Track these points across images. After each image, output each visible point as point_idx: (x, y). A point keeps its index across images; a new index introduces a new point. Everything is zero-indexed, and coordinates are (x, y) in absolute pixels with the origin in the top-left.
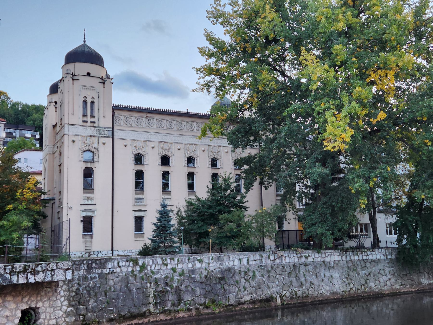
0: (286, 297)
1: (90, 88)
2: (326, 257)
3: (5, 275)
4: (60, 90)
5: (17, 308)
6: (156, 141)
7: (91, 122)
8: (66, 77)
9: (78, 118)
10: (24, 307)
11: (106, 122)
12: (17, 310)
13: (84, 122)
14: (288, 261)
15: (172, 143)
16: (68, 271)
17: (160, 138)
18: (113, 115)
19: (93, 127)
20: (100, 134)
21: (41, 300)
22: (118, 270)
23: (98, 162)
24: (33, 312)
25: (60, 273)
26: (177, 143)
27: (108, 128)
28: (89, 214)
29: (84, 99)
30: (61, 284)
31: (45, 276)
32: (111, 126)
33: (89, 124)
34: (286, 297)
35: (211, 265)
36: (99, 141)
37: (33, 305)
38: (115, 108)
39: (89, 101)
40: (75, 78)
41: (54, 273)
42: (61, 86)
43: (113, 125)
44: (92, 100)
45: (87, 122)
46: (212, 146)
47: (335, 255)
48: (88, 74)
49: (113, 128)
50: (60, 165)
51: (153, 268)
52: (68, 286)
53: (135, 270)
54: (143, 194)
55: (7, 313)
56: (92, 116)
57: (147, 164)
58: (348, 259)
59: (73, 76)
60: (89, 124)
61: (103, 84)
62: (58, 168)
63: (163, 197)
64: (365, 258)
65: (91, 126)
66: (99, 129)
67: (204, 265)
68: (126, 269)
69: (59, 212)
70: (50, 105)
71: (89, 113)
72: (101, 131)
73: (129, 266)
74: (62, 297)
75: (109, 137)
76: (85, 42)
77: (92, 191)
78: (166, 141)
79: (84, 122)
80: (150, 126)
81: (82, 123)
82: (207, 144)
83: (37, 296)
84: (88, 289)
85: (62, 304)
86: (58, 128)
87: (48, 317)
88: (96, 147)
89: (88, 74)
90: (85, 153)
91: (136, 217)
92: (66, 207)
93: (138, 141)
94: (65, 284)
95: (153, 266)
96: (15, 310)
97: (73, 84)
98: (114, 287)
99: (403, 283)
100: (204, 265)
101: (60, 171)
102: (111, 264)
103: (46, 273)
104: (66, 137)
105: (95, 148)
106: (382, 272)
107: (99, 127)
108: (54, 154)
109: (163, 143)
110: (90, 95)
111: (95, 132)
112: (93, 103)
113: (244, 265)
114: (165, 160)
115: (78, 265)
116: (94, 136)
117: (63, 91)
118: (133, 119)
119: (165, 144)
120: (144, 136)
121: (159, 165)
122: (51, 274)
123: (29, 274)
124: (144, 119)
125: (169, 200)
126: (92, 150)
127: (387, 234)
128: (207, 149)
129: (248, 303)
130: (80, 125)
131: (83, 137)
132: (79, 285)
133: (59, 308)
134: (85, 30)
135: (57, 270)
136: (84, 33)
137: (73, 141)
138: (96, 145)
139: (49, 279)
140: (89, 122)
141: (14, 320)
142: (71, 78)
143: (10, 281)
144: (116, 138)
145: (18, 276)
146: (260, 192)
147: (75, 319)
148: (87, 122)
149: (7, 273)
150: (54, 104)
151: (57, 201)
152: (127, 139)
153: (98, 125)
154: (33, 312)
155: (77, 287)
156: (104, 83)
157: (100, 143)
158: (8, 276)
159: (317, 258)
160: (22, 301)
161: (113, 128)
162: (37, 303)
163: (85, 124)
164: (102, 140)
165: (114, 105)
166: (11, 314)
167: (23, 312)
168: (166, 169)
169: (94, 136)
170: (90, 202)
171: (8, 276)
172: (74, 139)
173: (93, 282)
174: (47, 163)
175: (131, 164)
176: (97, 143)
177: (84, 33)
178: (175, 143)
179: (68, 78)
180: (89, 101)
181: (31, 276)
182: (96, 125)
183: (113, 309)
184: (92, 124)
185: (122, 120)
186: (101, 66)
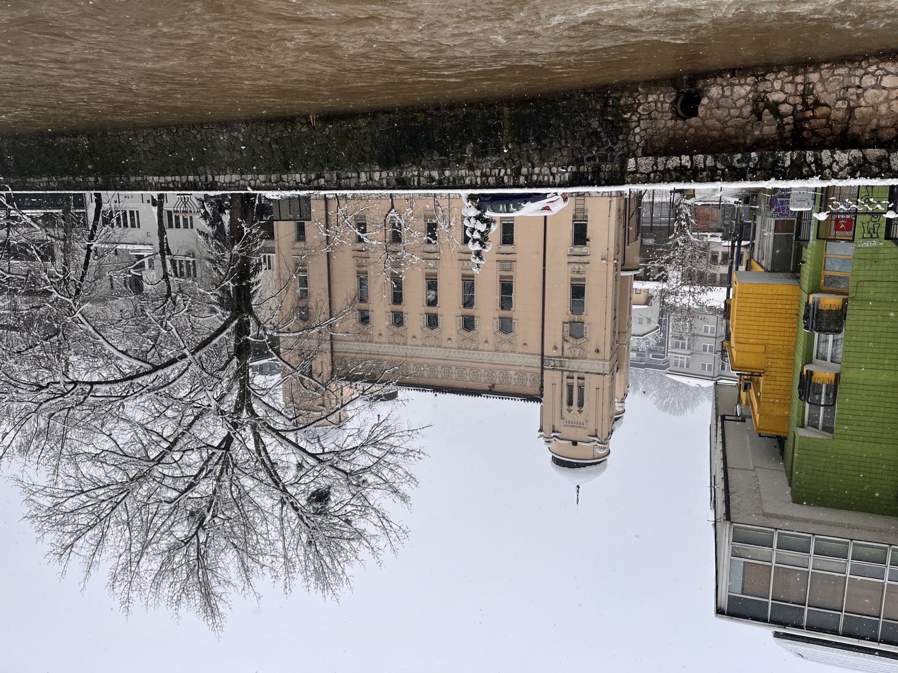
0: (301, 123)
2: (239, 181)
3: (723, 167)
5: (703, 119)
7: (572, 378)
9: (591, 383)
10: (693, 121)
13: (583, 379)
14: (298, 176)
15: (459, 348)
16: (632, 170)
17: (475, 355)
18: (542, 387)
19: (569, 371)
20: (560, 361)
21: (669, 129)
22: (554, 170)
23: (564, 323)
24: (680, 113)
25: (644, 168)
26: (451, 348)
28: (577, 250)
30: (640, 151)
31: (665, 164)
33: (576, 375)
34: (301, 123)
35: (416, 173)
37: (680, 123)
38: (534, 398)
39: (575, 407)
43: (542, 373)
47: (224, 183)
48: (575, 443)
49: (542, 369)
51: (503, 171)
52: (628, 149)
53: (530, 169)
54: (501, 277)
55: (719, 112)
56: (570, 387)
57: (457, 316)
58: (203, 178)
60: (576, 375)
64: (178, 178)
65: (574, 371)
67: (426, 173)
68: (543, 170)
72: (558, 365)
73: (538, 175)
74: (638, 134)
75: (547, 356)
77: (573, 283)
78: (467, 351)
79: (583, 379)
80: (491, 372)
81: (586, 376)
83: (674, 136)
84: (600, 144)
85: (639, 123)
87: (659, 105)
88: (566, 343)
92: (609, 259)
93: (506, 352)
94: (634, 151)
95: (502, 174)
98: (561, 144)
99: (117, 138)
100: (426, 173)
102: (564, 178)
104: (608, 356)
105: (567, 341)
106: (150, 156)
107: (563, 371)
109: (472, 348)
110: (574, 415)
112: (570, 403)
113: (366, 172)
115: (614, 178)
116: (569, 358)
120: (499, 358)
122: (658, 167)
123: (689, 167)
124: (497, 381)
126: (572, 338)
127: (137, 212)
129: (360, 116)
130: (587, 373)
132: (611, 149)
133: (642, 117)
137: (598, 351)
138: (567, 346)
139: (661, 160)
140: (576, 378)
143: (716, 159)
144: (538, 355)
147: (620, 100)
148: (579, 378)
149: (720, 169)
154: (680, 113)
155: (615, 147)
158: (719, 165)
159: (252, 180)
160: (696, 128)
162: (675, 126)
163: (581, 375)
168: (468, 311)
169: (569, 358)
170: (576, 266)
171: (719, 165)
173: (592, 153)
176: (565, 348)
178: (455, 348)
180: (575, 407)
181: (687, 164)
182: (566, 374)
183: (563, 113)
184: (571, 374)
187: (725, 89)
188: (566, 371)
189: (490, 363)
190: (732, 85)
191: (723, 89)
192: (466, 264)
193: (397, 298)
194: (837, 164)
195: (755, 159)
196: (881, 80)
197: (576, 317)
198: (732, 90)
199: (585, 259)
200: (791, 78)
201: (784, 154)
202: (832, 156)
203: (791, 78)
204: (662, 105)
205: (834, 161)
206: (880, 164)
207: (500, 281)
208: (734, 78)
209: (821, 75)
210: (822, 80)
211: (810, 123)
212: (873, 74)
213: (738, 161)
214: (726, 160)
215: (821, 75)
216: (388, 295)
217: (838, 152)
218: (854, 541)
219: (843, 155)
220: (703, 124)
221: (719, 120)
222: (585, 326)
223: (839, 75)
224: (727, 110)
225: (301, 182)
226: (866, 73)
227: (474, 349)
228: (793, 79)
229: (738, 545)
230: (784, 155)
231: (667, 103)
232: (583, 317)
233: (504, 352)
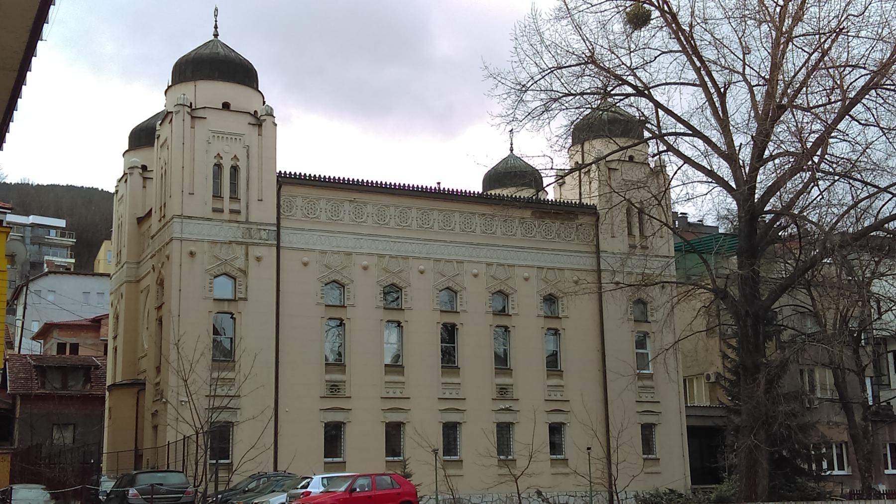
1: (221, 136)
4: (162, 140)
6: (373, 254)
7: (232, 211)
8: (177, 112)
17: (381, 247)
19: (237, 222)
20: (251, 238)
26: (419, 258)
27: (267, 224)
28: (224, 417)
32: (275, 222)
33: (226, 215)
36: (247, 254)
38: (286, 180)
42: (163, 132)
43: (278, 219)
45: (221, 211)
46: (494, 266)
48: (226, 106)
49: (278, 225)
50: (159, 308)
56: (234, 197)
60: (226, 215)
61: (257, 128)
62: (154, 315)
63: (328, 377)
65: (230, 221)
66: (246, 226)
69: (155, 414)
70: (131, 174)
71: (636, 232)
75: (271, 245)
76: (216, 35)
79: (215, 210)
81: (211, 215)
86: (154, 223)
88: (242, 267)
89: (226, 106)
90: (217, 279)
91: (327, 425)
93: (333, 252)
101: (160, 321)
104: (175, 244)
105: (240, 270)
108: (139, 281)
110: (229, 151)
111: (239, 234)
112: (235, 170)
117: (169, 142)
118: (413, 215)
125: (400, 385)
128: (484, 270)
131: (213, 245)
134: (216, 10)
136: (216, 16)
138: (240, 263)
140: (226, 211)
142: (188, 113)
146: (600, 367)
148: (221, 211)
150: (141, 171)
151: (149, 388)
153: (247, 219)
156: (260, 126)
161: (278, 225)
163: (217, 216)
164: (254, 251)
165: (280, 171)
172: (193, 249)
174: (123, 301)
177: (216, 16)
178: (414, 258)
179: (181, 113)
182: (242, 218)
184: (234, 217)
185: (299, 208)
186: (252, 87)
188: (242, 223)
222: (542, 313)
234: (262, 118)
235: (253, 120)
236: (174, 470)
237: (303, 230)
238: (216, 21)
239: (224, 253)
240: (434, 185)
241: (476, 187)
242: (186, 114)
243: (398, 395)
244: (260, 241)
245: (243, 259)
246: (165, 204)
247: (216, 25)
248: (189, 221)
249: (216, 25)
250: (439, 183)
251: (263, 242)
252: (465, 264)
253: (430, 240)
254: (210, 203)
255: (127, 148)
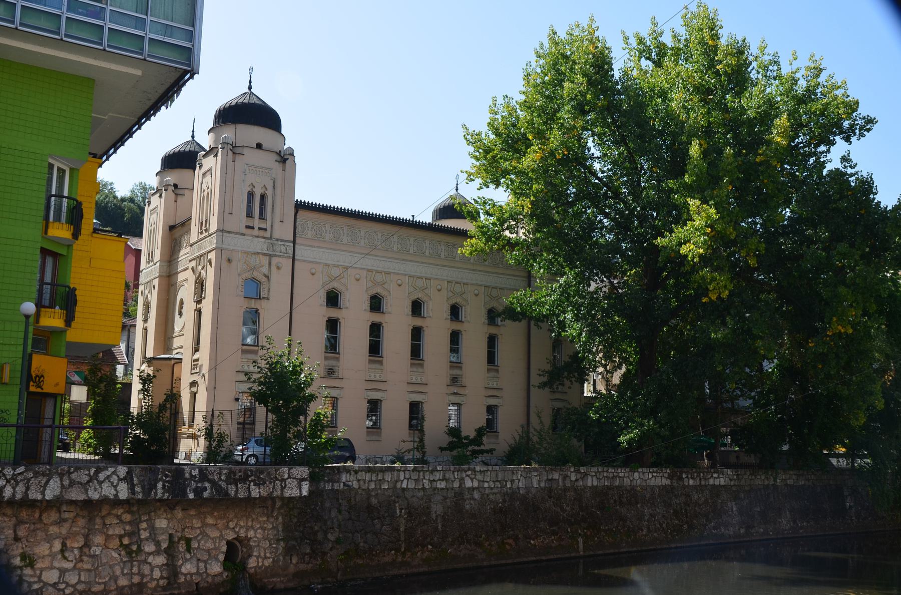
1: (254, 169)
3: (220, 483)
6: (481, 285)
7: (260, 229)
10: (231, 536)
11: (284, 231)
12: (222, 540)
13: (247, 227)
15: (389, 273)
16: (304, 483)
23: (268, 299)
26: (398, 274)
29: (249, 189)
30: (278, 504)
36: (270, 264)
38: (301, 206)
40: (237, 150)
41: (286, 485)
44: (262, 191)
45: (253, 228)
48: (259, 146)
49: (294, 242)
56: (262, 216)
59: (233, 147)
60: (256, 232)
61: (281, 165)
65: (258, 237)
78: (380, 269)
79: (247, 227)
82: (446, 278)
83: (247, 518)
87: (262, 554)
88: (266, 273)
89: (259, 146)
93: (335, 266)
96: (219, 540)
97: (234, 161)
103: (274, 484)
111: (265, 247)
112: (263, 197)
114: (376, 304)
119: (378, 274)
120: (344, 259)
121: (365, 310)
122: (281, 485)
123: (252, 483)
135: (289, 480)
138: (265, 270)
140: (256, 228)
141: (218, 555)
144: (299, 260)
145: (237, 486)
149: (223, 481)
150: (173, 188)
152: (316, 263)
157: (274, 268)
163: (249, 231)
166: (213, 546)
167: (229, 543)
171: (223, 485)
175: (321, 305)
178: (394, 273)
184: (262, 233)
187: (204, 570)
188: (267, 238)
189: (354, 252)
190: (198, 573)
191: (206, 569)
192: (378, 375)
193: (455, 337)
194: (112, 483)
195: (190, 491)
196: (60, 578)
197: (253, 306)
198: (198, 569)
199: (412, 388)
200: (145, 580)
201: (163, 496)
202: (117, 492)
203: (145, 580)
204: (259, 553)
205: (115, 487)
206: (70, 482)
207: (338, 353)
208: (197, 581)
209: (116, 584)
210: (115, 579)
211: (125, 530)
212: (68, 585)
213: (206, 489)
214: (217, 491)
215: (116, 584)
216: (466, 342)
217: (112, 497)
218: (101, 48)
219: (107, 494)
220: (221, 532)
221: (207, 535)
222: (242, 294)
223: (99, 584)
224: (201, 547)
225: (592, 476)
226: (73, 586)
227: (371, 271)
228: (142, 579)
229: (187, 44)
230: (163, 494)
231: (255, 556)
232: (245, 304)
233: (338, 266)
234: (286, 157)
235: (279, 158)
236: (11, 428)
237: (312, 246)
238: (251, 77)
239: (254, 261)
240: (409, 218)
241: (427, 218)
242: (229, 151)
243: (378, 378)
244: (280, 254)
245: (267, 266)
246: (206, 221)
247: (250, 80)
248: (228, 234)
249: (250, 80)
250: (413, 216)
251: (282, 254)
252: (392, 275)
253: (407, 260)
254: (245, 221)
255: (159, 169)
